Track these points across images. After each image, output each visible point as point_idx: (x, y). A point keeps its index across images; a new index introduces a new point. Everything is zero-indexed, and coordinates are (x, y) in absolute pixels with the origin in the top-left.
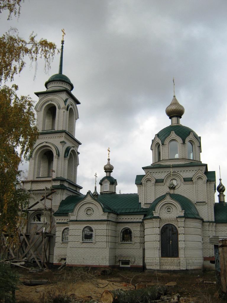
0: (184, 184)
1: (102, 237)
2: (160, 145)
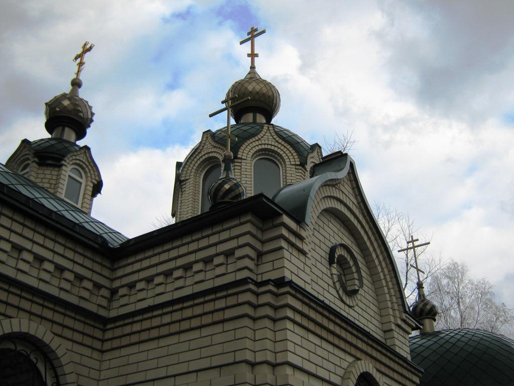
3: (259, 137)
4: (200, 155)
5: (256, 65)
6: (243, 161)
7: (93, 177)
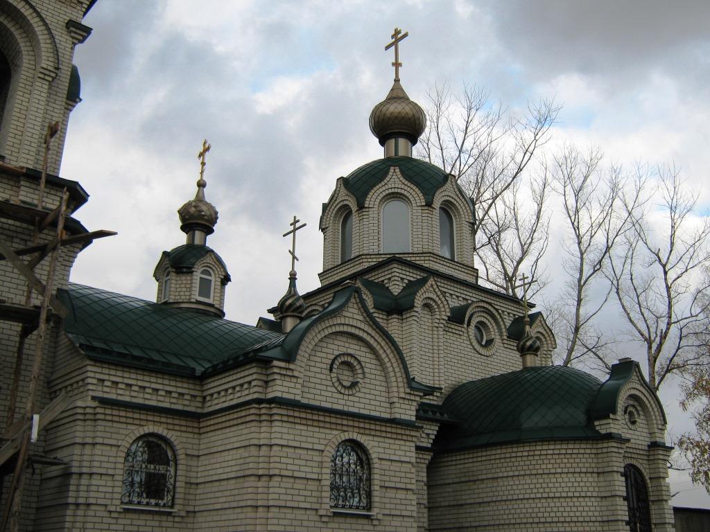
0: (506, 346)
1: (401, 495)
2: (350, 212)
3: (386, 181)
4: (336, 203)
5: (400, 77)
6: (371, 209)
7: (220, 273)
